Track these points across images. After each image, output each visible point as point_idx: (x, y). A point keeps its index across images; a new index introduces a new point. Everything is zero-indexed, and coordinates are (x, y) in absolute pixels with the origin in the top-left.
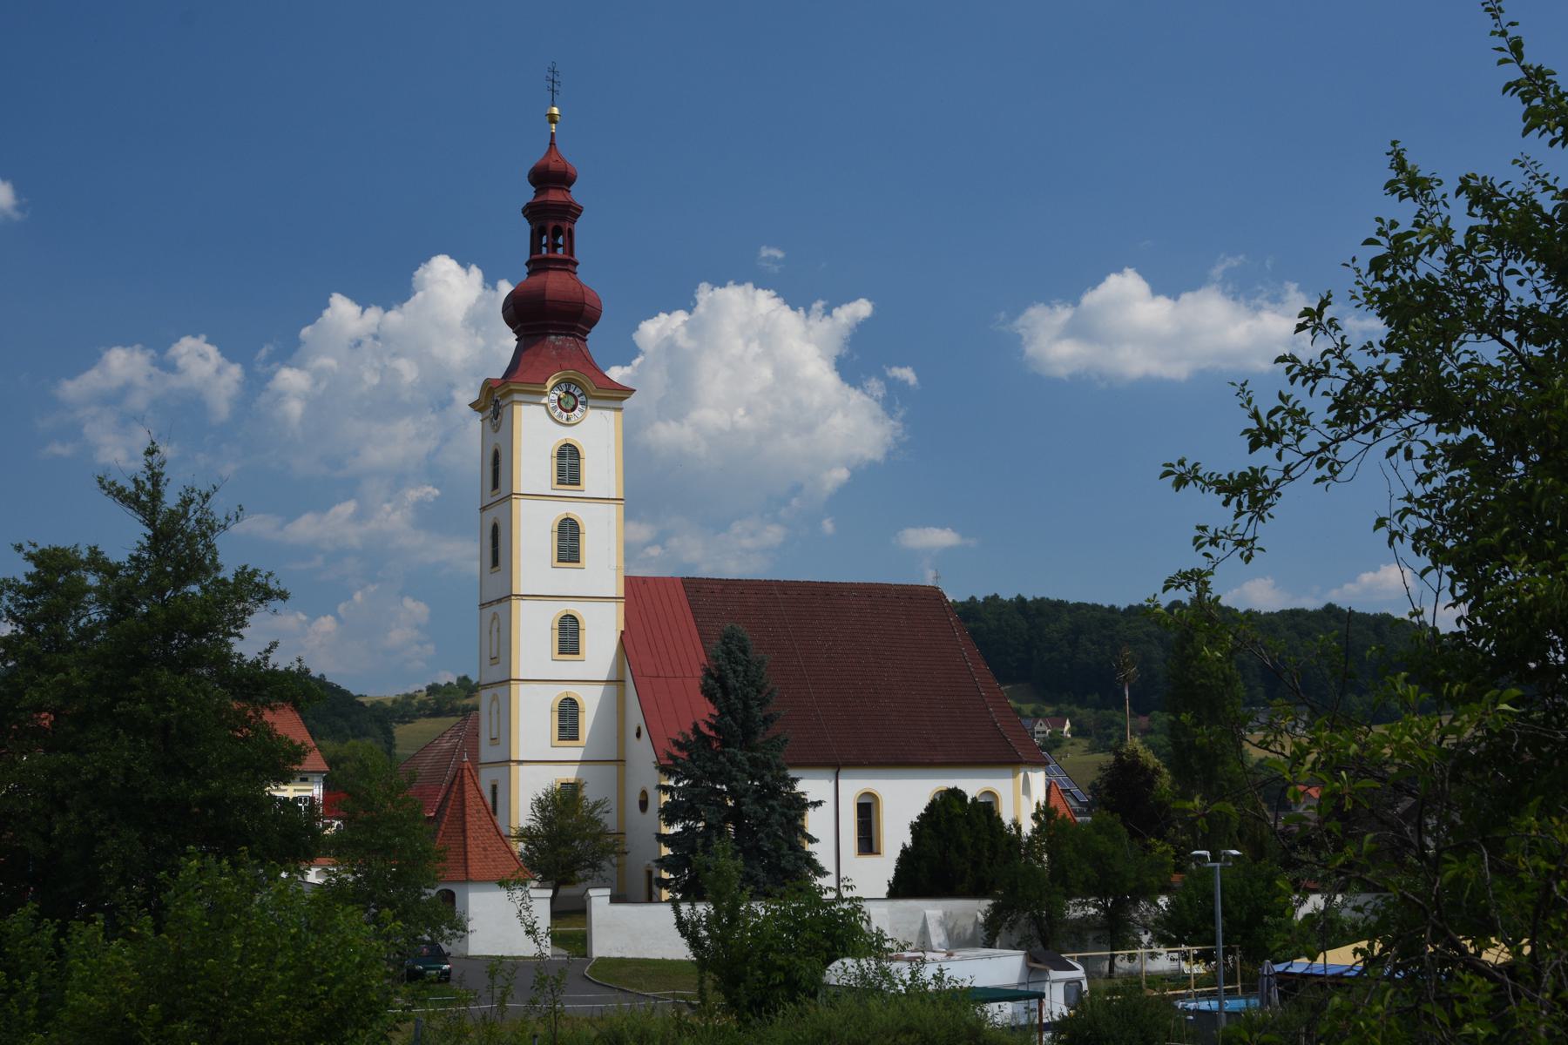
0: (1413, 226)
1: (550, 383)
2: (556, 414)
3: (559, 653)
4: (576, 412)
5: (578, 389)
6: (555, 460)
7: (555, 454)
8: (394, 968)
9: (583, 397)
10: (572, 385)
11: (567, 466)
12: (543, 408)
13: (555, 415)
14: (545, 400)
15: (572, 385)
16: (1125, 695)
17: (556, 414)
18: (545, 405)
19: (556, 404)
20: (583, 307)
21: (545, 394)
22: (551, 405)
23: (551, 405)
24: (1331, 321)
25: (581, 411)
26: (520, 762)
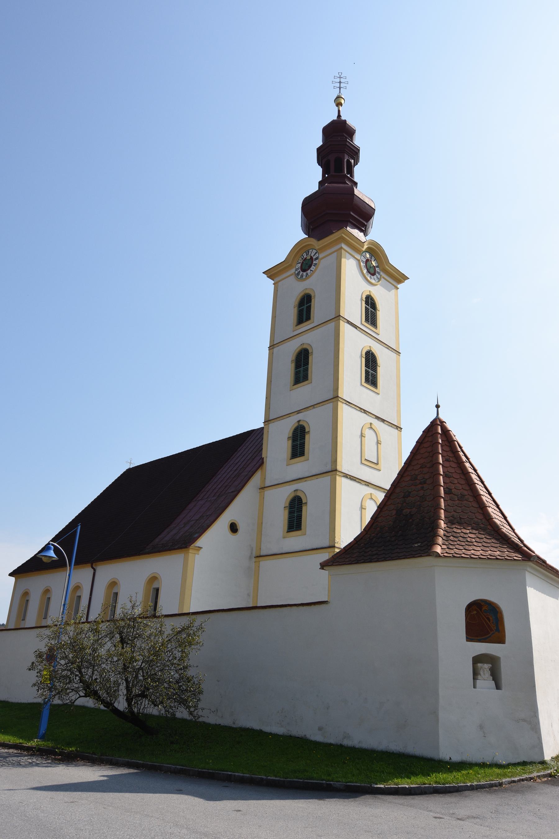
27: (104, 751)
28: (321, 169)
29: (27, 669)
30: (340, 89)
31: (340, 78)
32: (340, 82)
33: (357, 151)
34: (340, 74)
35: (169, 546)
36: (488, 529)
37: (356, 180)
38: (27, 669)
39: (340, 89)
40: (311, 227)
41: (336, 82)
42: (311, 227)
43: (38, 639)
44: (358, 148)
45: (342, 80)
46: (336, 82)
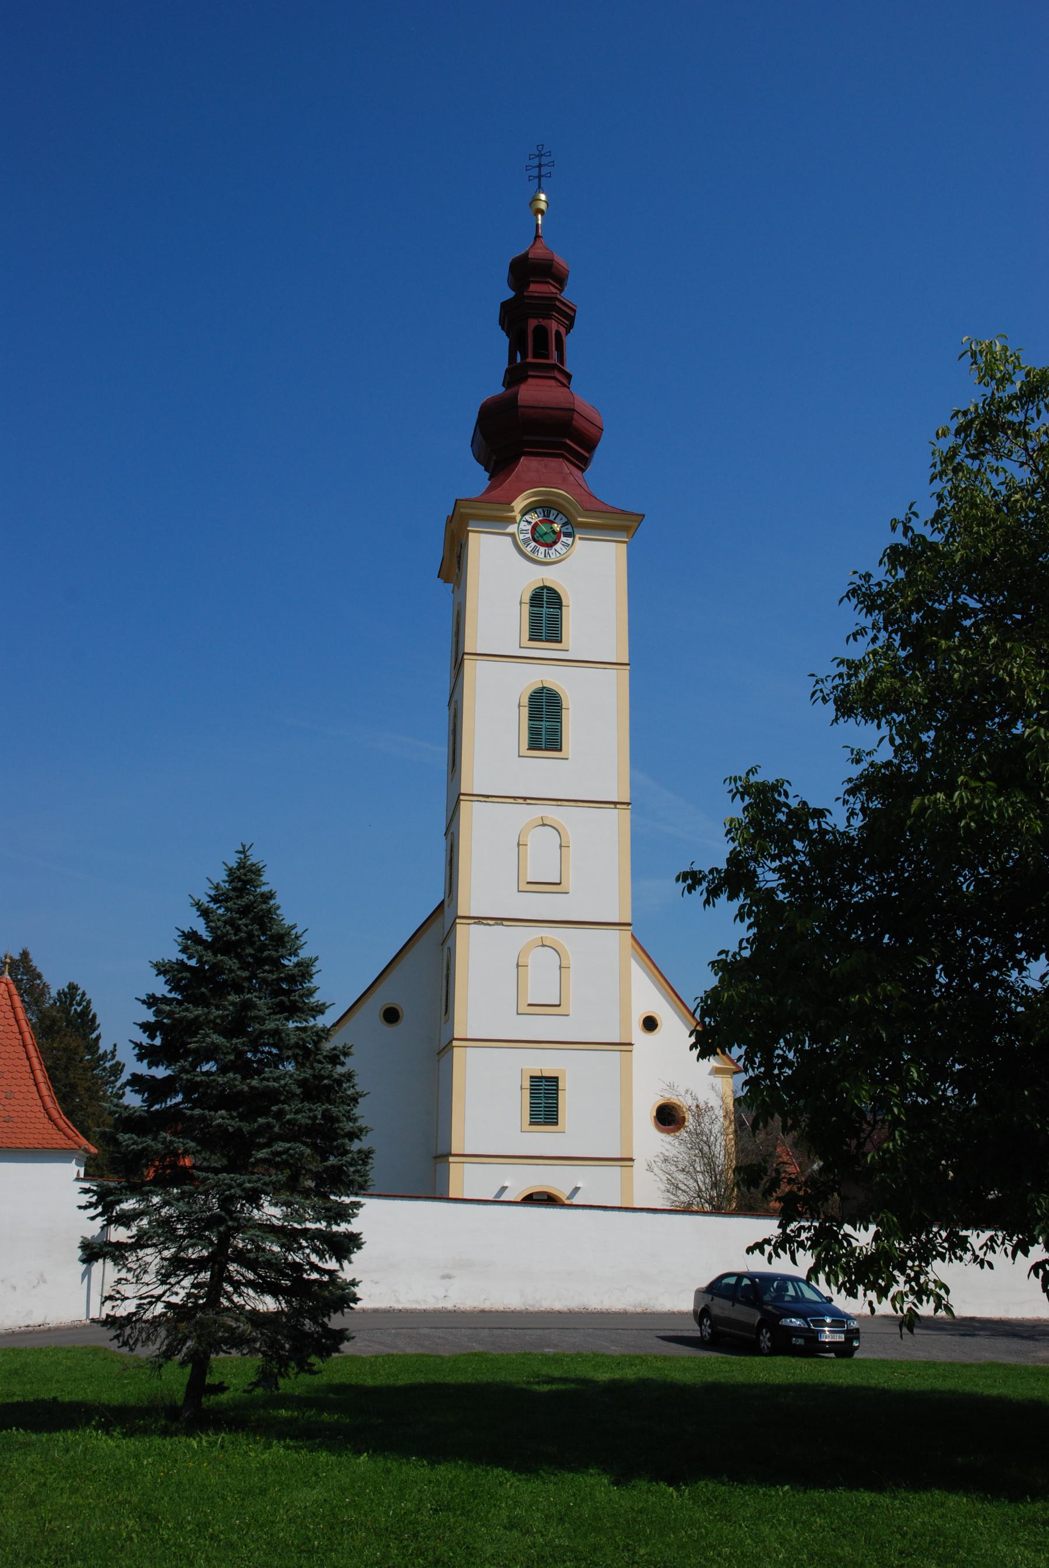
0: (718, 1054)
1: (519, 503)
2: (529, 549)
3: (529, 749)
4: (558, 546)
5: (560, 516)
6: (526, 608)
7: (527, 599)
8: (147, 1166)
9: (569, 526)
10: (553, 511)
11: (544, 730)
12: (509, 539)
13: (528, 550)
14: (512, 529)
15: (553, 511)
16: (550, 1391)
17: (529, 549)
18: (512, 535)
19: (529, 535)
20: (572, 418)
21: (512, 520)
22: (522, 536)
23: (522, 536)
24: (858, 761)
25: (566, 545)
26: (480, 920)
27: (971, 736)
28: (507, 340)
29: (1029, 1276)
30: (540, 180)
31: (540, 156)
32: (540, 166)
33: (572, 314)
34: (540, 148)
35: (348, 1158)
36: (304, 1414)
37: (568, 368)
38: (1029, 1276)
39: (540, 180)
40: (495, 458)
41: (533, 167)
42: (495, 458)
43: (681, 885)
44: (567, 310)
45: (545, 160)
46: (533, 167)
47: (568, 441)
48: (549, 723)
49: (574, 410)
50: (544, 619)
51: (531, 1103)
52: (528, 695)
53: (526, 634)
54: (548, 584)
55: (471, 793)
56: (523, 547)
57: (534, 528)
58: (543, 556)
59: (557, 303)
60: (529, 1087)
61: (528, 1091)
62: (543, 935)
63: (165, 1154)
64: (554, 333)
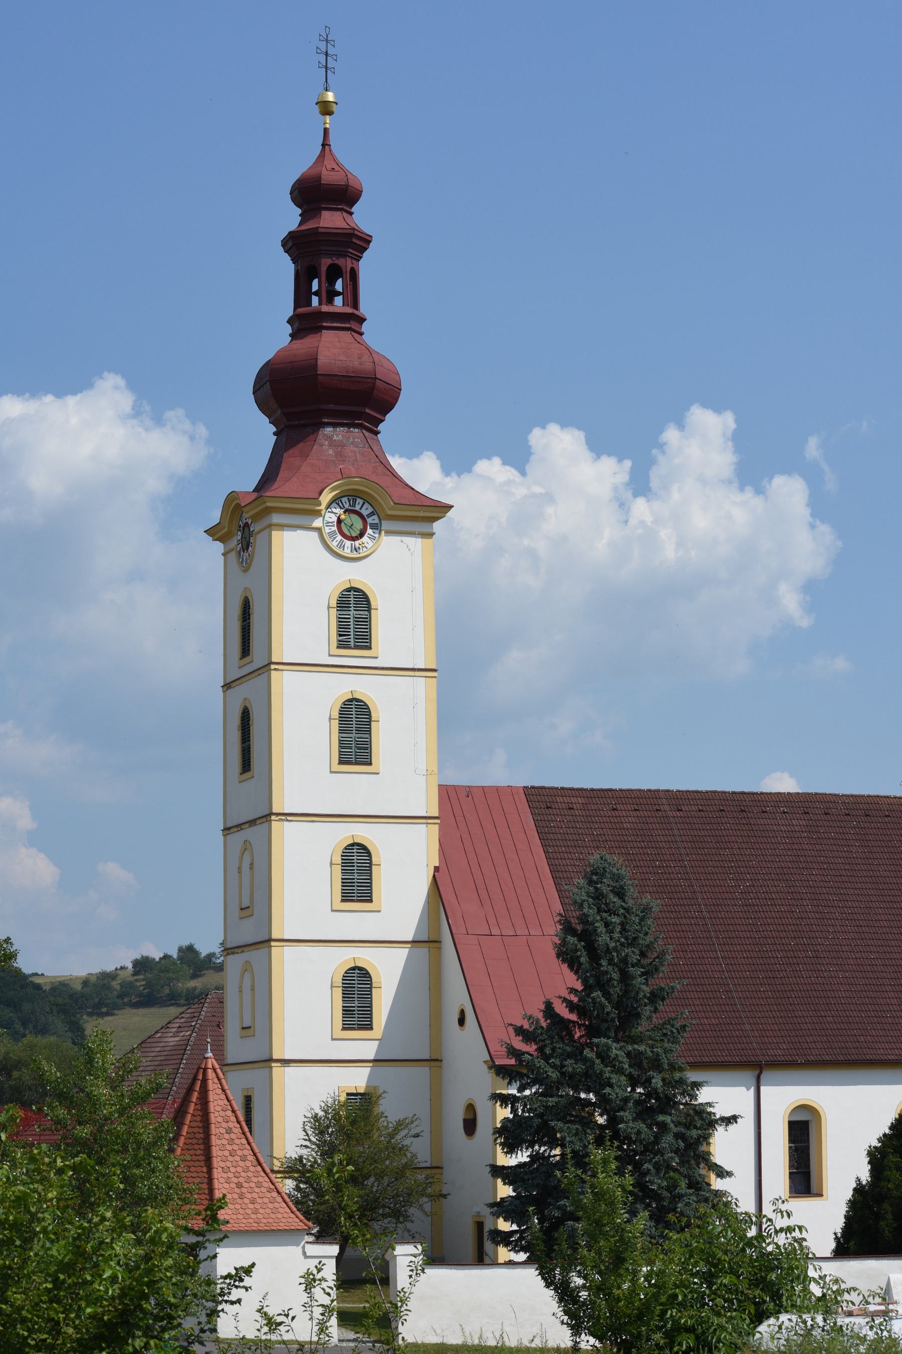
1: (326, 497)
5: (366, 505)
6: (334, 612)
7: (334, 603)
9: (375, 517)
10: (358, 500)
12: (315, 535)
13: (334, 544)
14: (318, 523)
15: (358, 500)
18: (319, 530)
21: (318, 513)
22: (327, 530)
25: (372, 538)
47: (367, 411)
48: (359, 612)
49: (376, 378)
50: (352, 627)
51: (343, 1007)
52: (340, 853)
53: (338, 896)
54: (360, 965)
55: (282, 812)
56: (328, 541)
57: (339, 521)
58: (349, 551)
59: (354, 240)
60: (340, 861)
61: (340, 867)
62: (351, 577)
63: (117, 1323)
64: (348, 269)
